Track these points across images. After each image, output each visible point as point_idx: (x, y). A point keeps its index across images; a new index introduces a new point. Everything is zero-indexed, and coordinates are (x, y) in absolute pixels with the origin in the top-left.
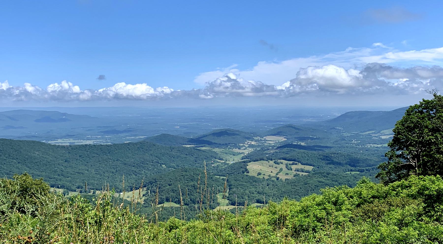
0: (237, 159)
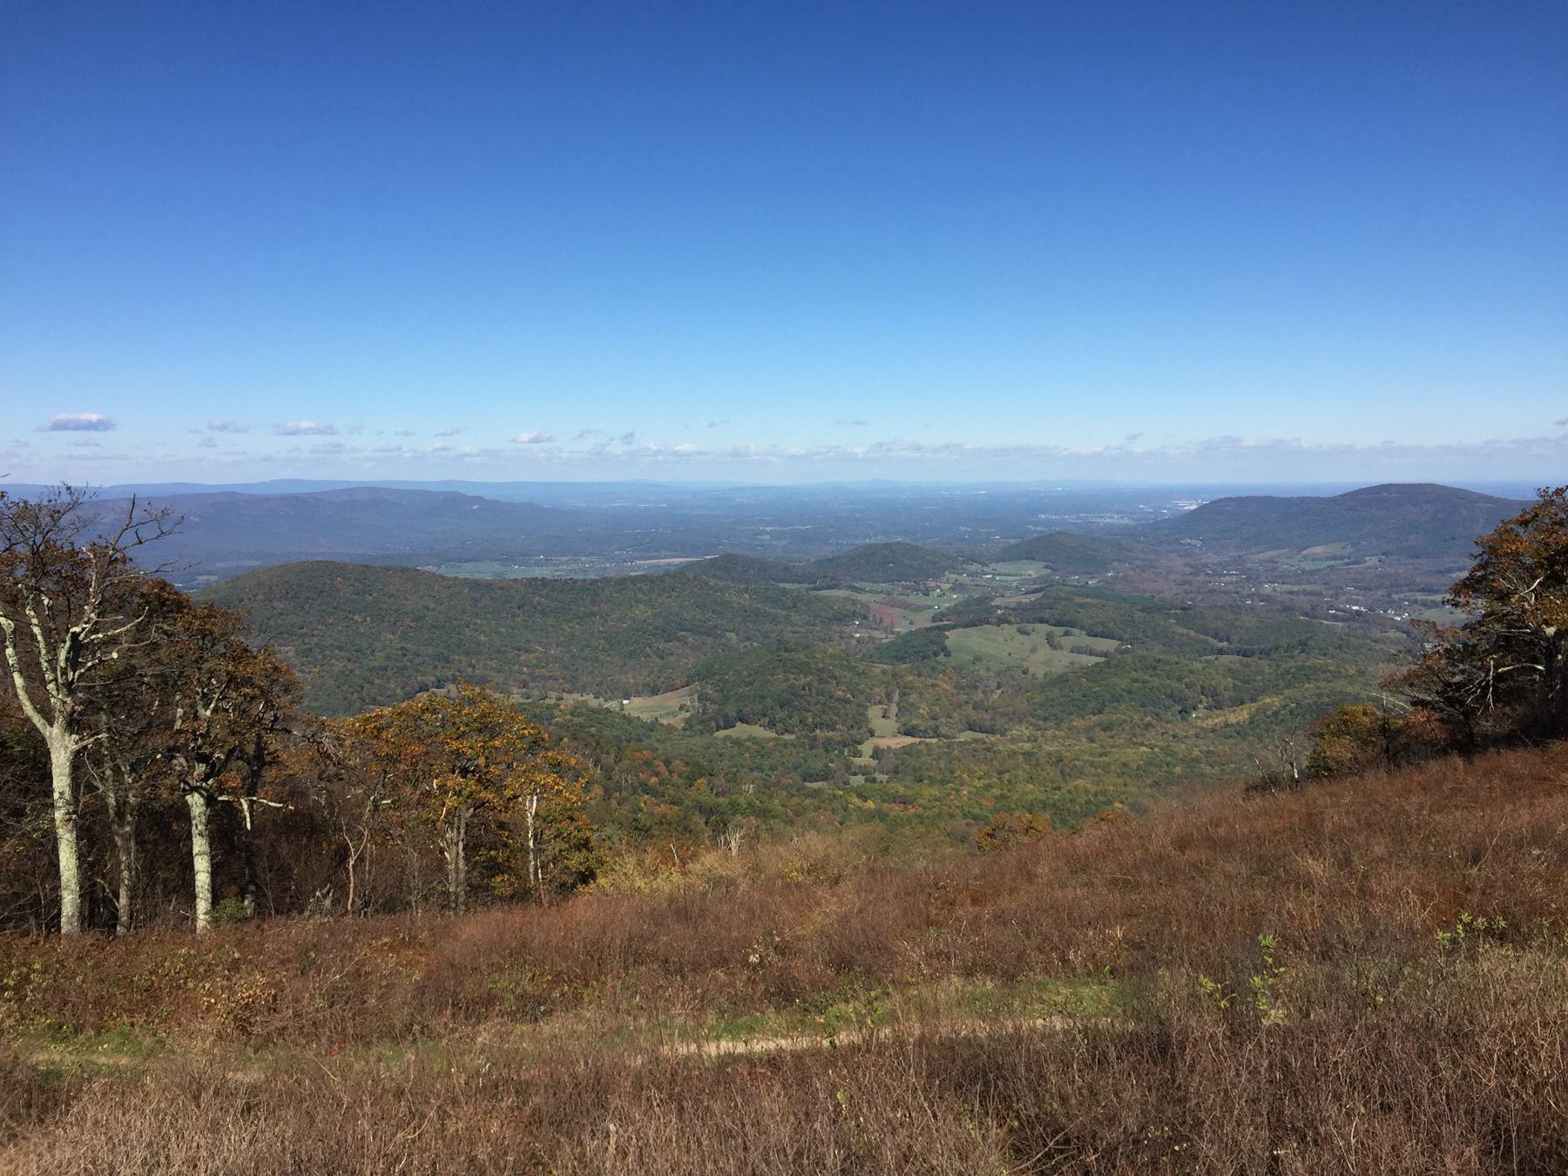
0: (923, 621)
